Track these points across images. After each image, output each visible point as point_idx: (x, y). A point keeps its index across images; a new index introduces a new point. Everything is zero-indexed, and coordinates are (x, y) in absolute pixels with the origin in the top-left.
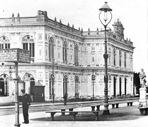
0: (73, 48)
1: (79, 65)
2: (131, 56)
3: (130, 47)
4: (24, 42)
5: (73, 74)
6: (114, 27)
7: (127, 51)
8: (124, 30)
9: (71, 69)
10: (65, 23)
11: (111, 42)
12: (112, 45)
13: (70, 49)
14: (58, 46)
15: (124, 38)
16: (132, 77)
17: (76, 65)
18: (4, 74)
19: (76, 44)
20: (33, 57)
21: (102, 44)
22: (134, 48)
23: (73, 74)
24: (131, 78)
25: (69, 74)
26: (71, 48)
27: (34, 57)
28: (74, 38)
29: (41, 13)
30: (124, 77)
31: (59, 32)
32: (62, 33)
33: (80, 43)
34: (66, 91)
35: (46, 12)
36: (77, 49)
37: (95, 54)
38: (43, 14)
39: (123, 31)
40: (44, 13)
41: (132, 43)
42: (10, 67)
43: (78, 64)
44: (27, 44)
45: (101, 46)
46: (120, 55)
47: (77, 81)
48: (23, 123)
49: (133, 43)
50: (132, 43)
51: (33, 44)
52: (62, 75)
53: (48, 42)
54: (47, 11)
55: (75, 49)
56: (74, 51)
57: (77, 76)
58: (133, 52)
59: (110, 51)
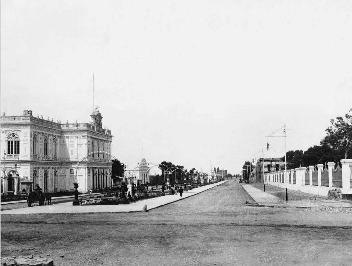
0: (53, 140)
1: (57, 159)
2: (109, 145)
3: (108, 136)
4: (10, 140)
5: (43, 168)
6: (92, 117)
7: (105, 141)
8: (102, 119)
9: (41, 163)
10: (45, 118)
11: (90, 134)
12: (91, 137)
13: (39, 142)
14: (40, 142)
15: (102, 128)
16: (110, 168)
17: (46, 158)
18: (12, 170)
19: (34, 133)
20: (11, 154)
21: (82, 137)
22: (112, 137)
23: (43, 168)
24: (110, 169)
25: (49, 168)
26: (41, 140)
27: (19, 154)
28: (53, 132)
29: (27, 112)
30: (98, 169)
31: (41, 128)
32: (43, 129)
33: (58, 136)
34: (46, 186)
35: (31, 111)
36: (56, 143)
37: (77, 149)
38: (28, 113)
39: (101, 120)
40: (29, 112)
41: (110, 131)
42: (15, 165)
43: (56, 158)
44: (12, 142)
45: (80, 139)
46: (98, 146)
47: (56, 175)
48: (268, 150)
49: (111, 132)
50: (110, 131)
51: (19, 142)
52: (43, 170)
53: (32, 139)
54: (32, 111)
55: (54, 143)
56: (43, 144)
57: (46, 170)
58: (111, 142)
59: (89, 144)
